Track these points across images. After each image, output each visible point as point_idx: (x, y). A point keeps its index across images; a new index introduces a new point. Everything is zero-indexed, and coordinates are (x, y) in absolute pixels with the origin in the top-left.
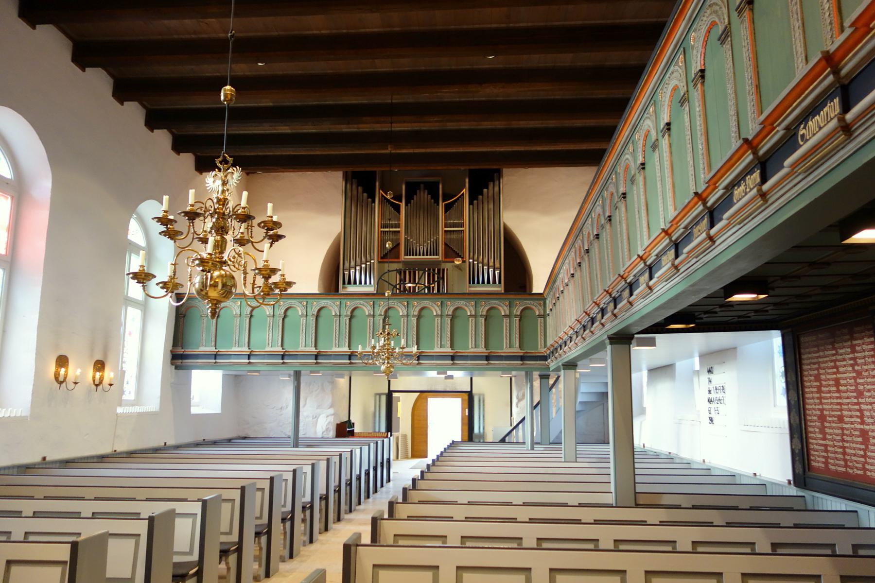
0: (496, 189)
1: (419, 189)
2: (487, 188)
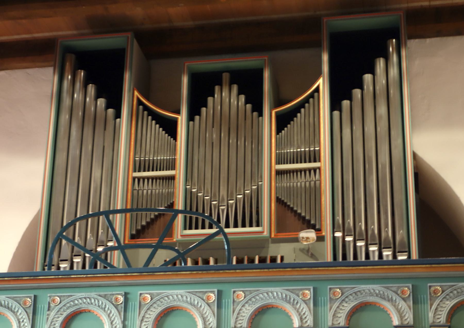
0: (393, 72)
1: (221, 84)
2: (372, 71)
